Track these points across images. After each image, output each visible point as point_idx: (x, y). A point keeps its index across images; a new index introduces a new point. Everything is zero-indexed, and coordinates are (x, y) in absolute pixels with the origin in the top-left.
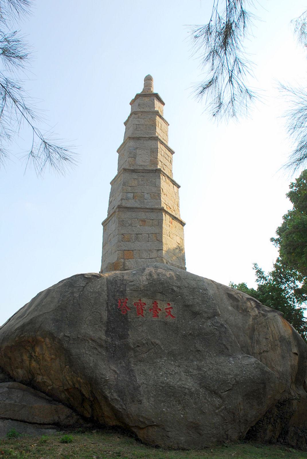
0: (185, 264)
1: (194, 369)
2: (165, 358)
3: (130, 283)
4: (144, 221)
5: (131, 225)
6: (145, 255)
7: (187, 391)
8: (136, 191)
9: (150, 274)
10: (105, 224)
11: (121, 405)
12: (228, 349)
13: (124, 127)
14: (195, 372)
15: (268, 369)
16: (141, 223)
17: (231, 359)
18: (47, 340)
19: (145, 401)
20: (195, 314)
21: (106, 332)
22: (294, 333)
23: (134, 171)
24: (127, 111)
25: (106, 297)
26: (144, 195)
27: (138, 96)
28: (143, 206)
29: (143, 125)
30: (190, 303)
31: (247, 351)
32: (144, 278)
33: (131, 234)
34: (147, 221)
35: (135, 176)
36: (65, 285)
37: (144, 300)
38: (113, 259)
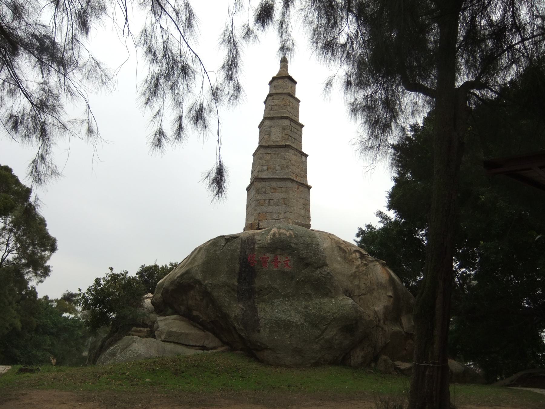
0: (310, 221)
1: (302, 308)
2: (281, 299)
3: (258, 242)
4: (274, 189)
5: (265, 192)
6: (275, 216)
7: (294, 324)
8: (270, 164)
9: (274, 235)
10: (248, 189)
11: (245, 333)
12: (332, 292)
13: (264, 105)
14: (303, 310)
15: (361, 309)
16: (273, 191)
17: (333, 300)
18: (197, 286)
19: (262, 331)
20: (307, 265)
21: (238, 279)
22: (391, 280)
23: (268, 147)
24: (266, 90)
25: (239, 253)
26: (275, 167)
27: (274, 79)
28: (274, 176)
29: (276, 105)
30: (304, 256)
31: (348, 293)
32: (269, 237)
33: (265, 200)
34: (277, 188)
35: (269, 151)
36: (211, 244)
37: (268, 255)
38: (251, 221)
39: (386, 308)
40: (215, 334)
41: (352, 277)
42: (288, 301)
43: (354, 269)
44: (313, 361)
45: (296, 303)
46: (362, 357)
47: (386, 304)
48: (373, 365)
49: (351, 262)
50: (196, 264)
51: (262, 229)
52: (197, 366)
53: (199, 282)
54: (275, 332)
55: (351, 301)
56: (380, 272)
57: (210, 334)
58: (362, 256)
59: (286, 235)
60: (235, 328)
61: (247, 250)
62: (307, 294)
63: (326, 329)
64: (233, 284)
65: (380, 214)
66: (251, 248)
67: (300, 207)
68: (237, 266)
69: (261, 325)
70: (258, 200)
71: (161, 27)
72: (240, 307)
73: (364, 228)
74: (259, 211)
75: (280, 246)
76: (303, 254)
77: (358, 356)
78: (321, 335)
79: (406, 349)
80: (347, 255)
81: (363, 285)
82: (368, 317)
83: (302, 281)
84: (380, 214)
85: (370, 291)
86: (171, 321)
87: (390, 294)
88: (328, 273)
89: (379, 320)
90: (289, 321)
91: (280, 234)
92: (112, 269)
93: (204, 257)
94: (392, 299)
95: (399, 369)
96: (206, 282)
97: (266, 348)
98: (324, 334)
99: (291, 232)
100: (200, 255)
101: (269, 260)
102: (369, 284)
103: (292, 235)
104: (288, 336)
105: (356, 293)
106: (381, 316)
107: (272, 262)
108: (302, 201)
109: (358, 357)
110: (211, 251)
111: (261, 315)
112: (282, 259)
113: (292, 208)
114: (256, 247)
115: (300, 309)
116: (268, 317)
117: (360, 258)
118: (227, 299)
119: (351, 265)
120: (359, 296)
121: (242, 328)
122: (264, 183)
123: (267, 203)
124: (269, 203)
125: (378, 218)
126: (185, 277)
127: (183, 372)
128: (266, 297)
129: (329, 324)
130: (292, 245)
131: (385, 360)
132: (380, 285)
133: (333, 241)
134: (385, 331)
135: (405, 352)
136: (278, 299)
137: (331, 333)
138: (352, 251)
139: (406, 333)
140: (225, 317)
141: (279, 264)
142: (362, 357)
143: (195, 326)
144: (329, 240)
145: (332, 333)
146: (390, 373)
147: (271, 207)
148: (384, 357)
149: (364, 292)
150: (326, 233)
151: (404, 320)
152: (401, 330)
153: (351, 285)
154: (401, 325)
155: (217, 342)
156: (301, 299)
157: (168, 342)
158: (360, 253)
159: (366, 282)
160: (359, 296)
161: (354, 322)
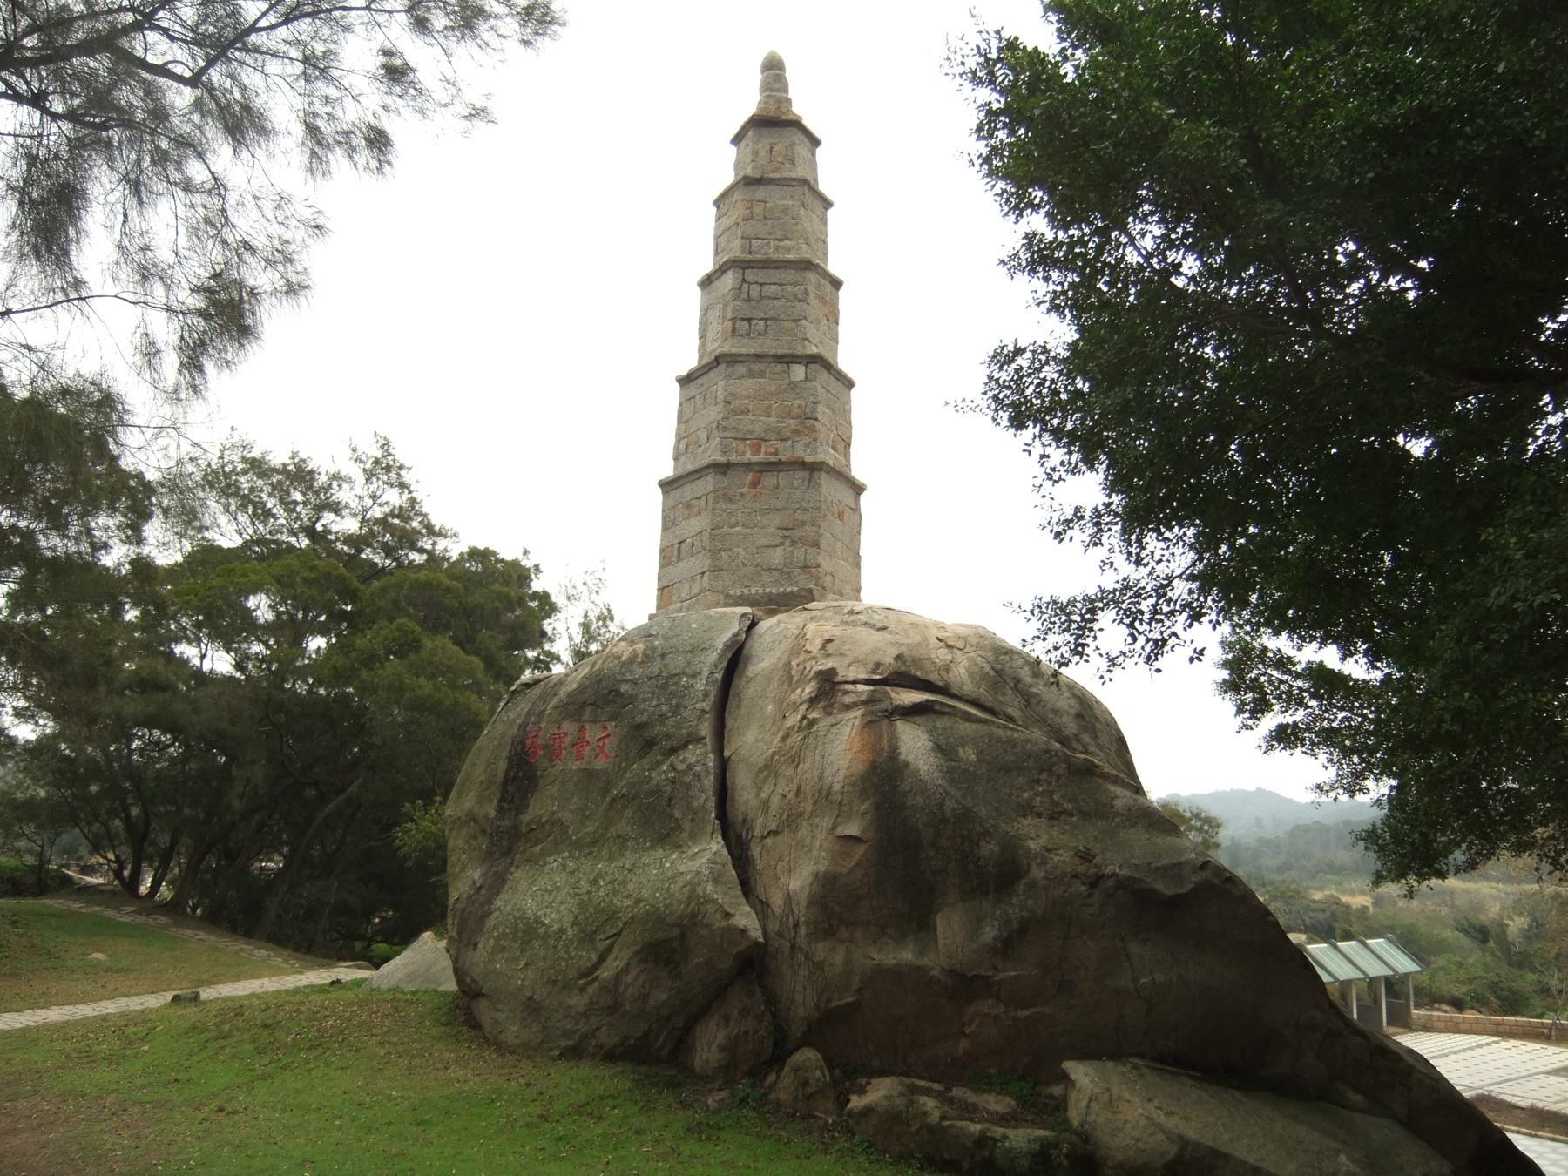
44: (565, 1043)
46: (722, 1049)
63: (609, 949)
68: (503, 766)
87: (853, 829)
89: (796, 926)
92: (1158, 671)
101: (568, 740)
106: (801, 910)
109: (709, 1046)
112: (593, 733)
129: (618, 935)
130: (624, 688)
149: (773, 827)
160: (763, 838)
161: (676, 931)
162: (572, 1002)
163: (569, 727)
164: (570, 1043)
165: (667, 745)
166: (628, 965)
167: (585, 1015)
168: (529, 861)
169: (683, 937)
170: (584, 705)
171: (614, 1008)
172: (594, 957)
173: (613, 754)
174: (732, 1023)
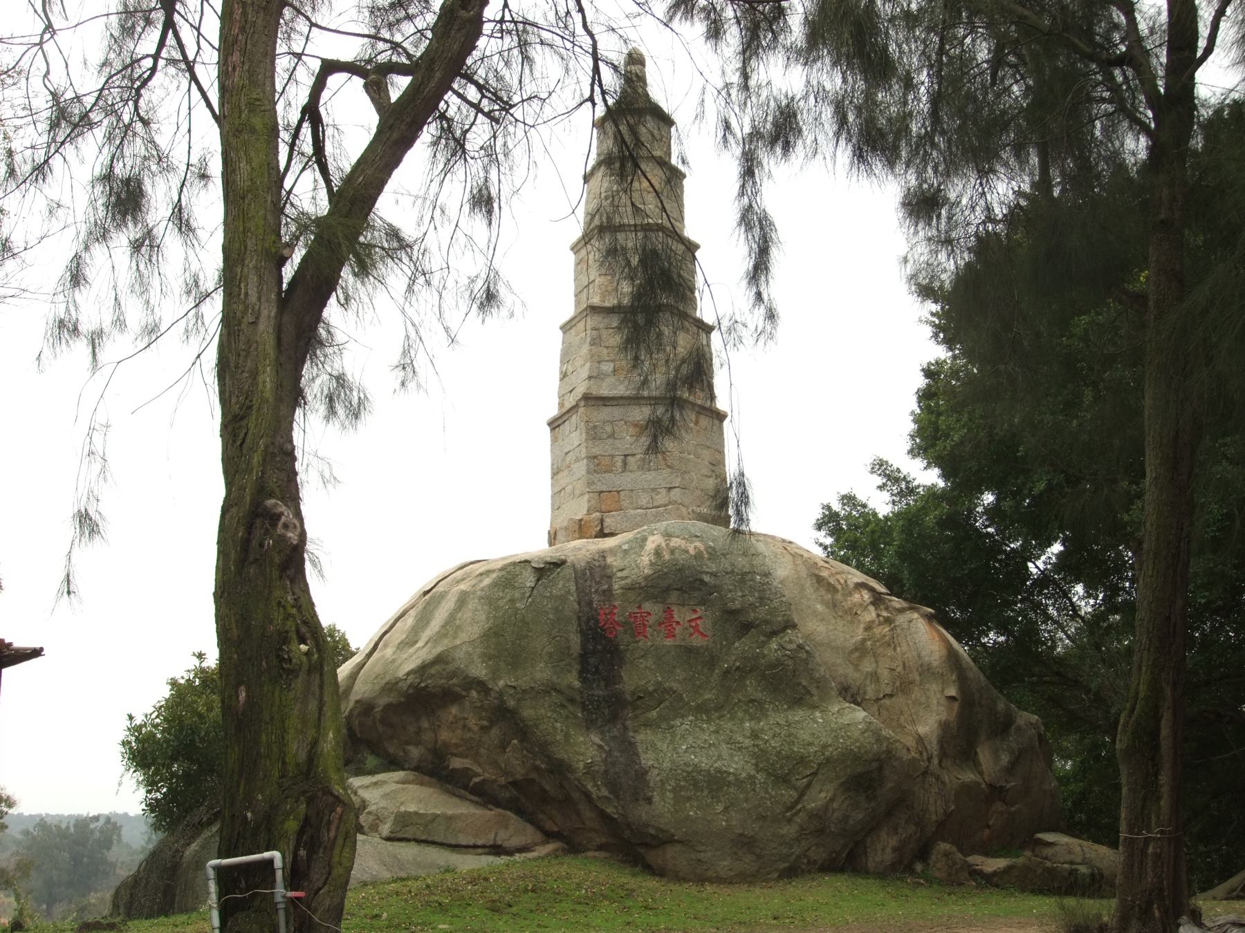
1: (745, 737)
2: (691, 718)
3: (619, 574)
5: (612, 436)
7: (731, 778)
9: (658, 552)
11: (616, 807)
12: (812, 695)
14: (747, 742)
18: (474, 694)
19: (656, 798)
21: (581, 673)
22: (952, 655)
25: (576, 606)
30: (737, 605)
31: (852, 695)
33: (613, 456)
37: (647, 606)
39: (944, 726)
40: (520, 812)
41: (857, 654)
42: (709, 721)
43: (860, 634)
44: (783, 866)
45: (730, 725)
47: (944, 717)
48: (919, 867)
49: (852, 614)
50: (464, 636)
51: (612, 535)
52: (533, 891)
53: (481, 686)
54: (689, 799)
55: (860, 714)
56: (923, 637)
57: (509, 813)
58: (877, 600)
59: (687, 552)
60: (587, 795)
61: (595, 597)
62: (753, 701)
63: (809, 785)
64: (570, 687)
65: (881, 467)
66: (604, 591)
67: (705, 471)
68: (575, 640)
69: (651, 784)
70: (595, 457)
71: (633, 204)
72: (594, 743)
73: (836, 507)
74: (599, 488)
75: (677, 583)
76: (733, 600)
77: (884, 847)
78: (797, 802)
79: (988, 826)
80: (839, 597)
81: (886, 672)
82: (905, 751)
83: (738, 668)
84: (881, 467)
85: (903, 686)
86: (394, 787)
87: (952, 692)
88: (800, 647)
89: (930, 759)
90: (719, 771)
91: (672, 552)
93: (483, 617)
94: (956, 705)
95: (981, 874)
96: (501, 683)
97: (671, 841)
98: (805, 798)
99: (698, 544)
100: (466, 614)
102: (899, 669)
103: (701, 552)
104: (720, 808)
105: (870, 692)
106: (934, 748)
107: (660, 624)
108: (706, 455)
109: (883, 850)
110: (501, 603)
111: (647, 759)
112: (682, 615)
113: (687, 476)
114: (616, 587)
115: (740, 739)
116: (667, 765)
117: (872, 603)
118: (559, 725)
119: (852, 622)
120: (878, 700)
121: (607, 794)
122: (608, 409)
123: (619, 464)
124: (625, 464)
125: (875, 476)
126: (433, 671)
127: (510, 906)
128: (654, 713)
129: (815, 774)
130: (706, 578)
131: (947, 854)
132: (926, 670)
133: (799, 562)
134: (943, 783)
135: (987, 832)
136: (683, 717)
137: (823, 795)
138: (851, 586)
139: (990, 786)
140: (560, 769)
141: (678, 630)
142: (895, 850)
143: (461, 797)
144: (788, 558)
145: (819, 797)
146: (960, 884)
147: (632, 476)
148: (944, 846)
149: (888, 691)
150: (773, 537)
151: (984, 755)
152: (978, 779)
153: (856, 675)
154: (976, 765)
155: (528, 834)
156: (740, 714)
157: (400, 840)
158: (872, 590)
159: (894, 665)
161: (875, 765)
162: (784, 831)
163: (653, 609)
164: (786, 865)
165: (768, 629)
166: (835, 795)
167: (797, 840)
168: (646, 725)
169: (880, 769)
170: (668, 589)
171: (821, 832)
172: (795, 795)
173: (709, 633)
174: (900, 830)
